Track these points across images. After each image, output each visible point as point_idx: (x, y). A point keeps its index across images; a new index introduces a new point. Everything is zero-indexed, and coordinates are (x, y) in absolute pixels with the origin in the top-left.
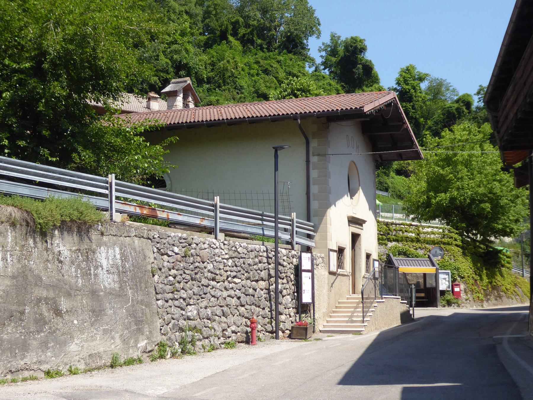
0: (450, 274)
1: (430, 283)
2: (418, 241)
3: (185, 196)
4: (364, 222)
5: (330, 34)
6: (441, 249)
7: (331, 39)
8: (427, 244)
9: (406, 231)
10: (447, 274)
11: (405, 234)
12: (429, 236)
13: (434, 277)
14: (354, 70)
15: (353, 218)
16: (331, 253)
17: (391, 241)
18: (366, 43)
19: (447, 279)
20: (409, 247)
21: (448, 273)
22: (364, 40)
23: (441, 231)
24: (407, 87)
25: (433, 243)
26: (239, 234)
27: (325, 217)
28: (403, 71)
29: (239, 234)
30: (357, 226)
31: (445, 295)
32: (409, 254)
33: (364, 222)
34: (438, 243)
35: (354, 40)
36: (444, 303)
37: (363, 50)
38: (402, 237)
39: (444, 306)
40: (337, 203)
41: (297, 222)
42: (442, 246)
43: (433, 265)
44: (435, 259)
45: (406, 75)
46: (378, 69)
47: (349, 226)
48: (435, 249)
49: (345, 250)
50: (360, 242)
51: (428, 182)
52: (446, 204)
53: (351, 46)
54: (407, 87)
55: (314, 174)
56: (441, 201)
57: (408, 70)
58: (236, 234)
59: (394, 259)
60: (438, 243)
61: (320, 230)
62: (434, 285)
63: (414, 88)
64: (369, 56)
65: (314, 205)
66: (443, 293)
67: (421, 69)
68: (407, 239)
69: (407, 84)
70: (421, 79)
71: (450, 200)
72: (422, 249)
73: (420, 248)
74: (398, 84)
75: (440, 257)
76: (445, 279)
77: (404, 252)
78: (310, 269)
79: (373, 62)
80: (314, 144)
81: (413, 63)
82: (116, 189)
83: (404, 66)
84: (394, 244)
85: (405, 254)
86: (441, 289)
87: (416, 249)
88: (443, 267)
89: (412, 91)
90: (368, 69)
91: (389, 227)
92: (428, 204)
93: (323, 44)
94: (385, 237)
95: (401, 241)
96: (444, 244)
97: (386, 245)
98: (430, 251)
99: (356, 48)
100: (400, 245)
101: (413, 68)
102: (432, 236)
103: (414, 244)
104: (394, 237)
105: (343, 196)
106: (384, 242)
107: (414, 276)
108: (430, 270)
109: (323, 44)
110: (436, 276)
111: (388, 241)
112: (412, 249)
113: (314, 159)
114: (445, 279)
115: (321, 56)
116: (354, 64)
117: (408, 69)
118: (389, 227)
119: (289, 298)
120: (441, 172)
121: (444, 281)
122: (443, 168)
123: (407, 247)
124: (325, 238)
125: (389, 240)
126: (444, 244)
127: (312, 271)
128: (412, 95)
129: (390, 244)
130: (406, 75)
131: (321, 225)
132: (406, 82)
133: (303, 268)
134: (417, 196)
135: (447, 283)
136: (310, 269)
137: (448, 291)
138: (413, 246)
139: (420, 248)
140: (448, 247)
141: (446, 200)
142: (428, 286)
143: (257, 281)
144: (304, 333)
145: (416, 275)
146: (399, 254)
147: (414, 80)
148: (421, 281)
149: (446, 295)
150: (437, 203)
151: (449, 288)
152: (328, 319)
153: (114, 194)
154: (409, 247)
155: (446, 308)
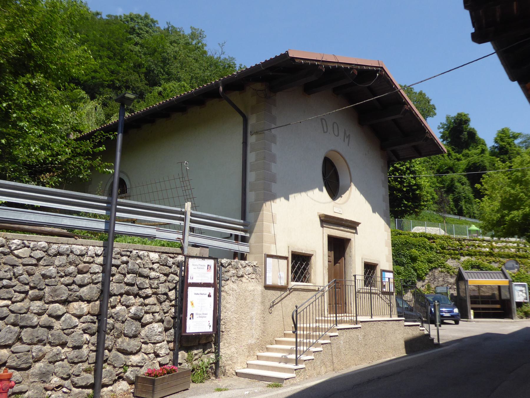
0: (527, 286)
1: (505, 295)
2: (491, 254)
3: (220, 217)
4: (358, 224)
5: (445, 116)
6: (517, 263)
7: (447, 120)
8: (501, 258)
9: (479, 246)
10: (524, 286)
11: (478, 249)
12: (502, 250)
13: (507, 290)
14: (461, 136)
15: (326, 216)
16: (269, 260)
17: (463, 256)
18: (469, 116)
19: (524, 291)
20: (483, 261)
21: (525, 285)
22: (468, 114)
23: (515, 245)
24: (503, 144)
25: (509, 256)
26: (43, 228)
27: (261, 212)
28: (500, 132)
29: (38, 228)
30: (342, 228)
31: (522, 306)
32: (483, 268)
33: (358, 224)
34: (513, 257)
35: (460, 115)
36: (521, 314)
37: (467, 121)
38: (475, 252)
39: (522, 318)
40: (291, 197)
41: (192, 215)
42: (517, 259)
43: (506, 277)
44: (507, 272)
45: (502, 135)
46: (481, 134)
47: (322, 226)
48: (511, 263)
49: (313, 258)
50: (350, 248)
51: (502, 202)
52: (519, 220)
53: (458, 119)
54: (503, 144)
55: (251, 157)
56: (513, 217)
57: (503, 131)
58: (27, 227)
59: (463, 272)
60: (513, 257)
61: (256, 229)
62: (508, 296)
63: (509, 144)
64: (472, 125)
65: (251, 196)
66: (519, 304)
67: (514, 129)
68: (481, 254)
69: (504, 142)
70: (515, 137)
71: (523, 217)
72: (496, 263)
73: (494, 261)
74: (496, 142)
75: (516, 270)
76: (521, 291)
77: (477, 266)
78: (212, 281)
79: (476, 129)
80: (252, 121)
81: (508, 126)
82: (191, 219)
83: (500, 129)
84: (467, 258)
85: (478, 267)
86: (517, 301)
87: (490, 263)
88: (519, 279)
89: (508, 146)
90: (472, 135)
91: (461, 243)
92: (500, 222)
93: (441, 124)
94: (457, 252)
95: (476, 255)
96: (520, 257)
97: (459, 259)
98: (504, 264)
99: (461, 120)
100: (473, 259)
101: (508, 130)
102: (507, 250)
103: (488, 258)
104: (467, 252)
105: (315, 188)
106: (456, 256)
107: (489, 288)
108: (503, 282)
109: (441, 124)
110: (510, 289)
111: (461, 256)
112: (486, 263)
113: (252, 139)
114: (521, 291)
115: (440, 132)
116: (461, 132)
117: (503, 131)
118: (461, 243)
119: (158, 327)
120: (512, 191)
121: (521, 293)
122: (513, 188)
123: (480, 261)
124: (261, 240)
125: (462, 254)
126: (520, 257)
127: (217, 286)
128: (507, 149)
129: (463, 259)
130: (502, 135)
131: (257, 223)
132: (502, 140)
133: (190, 281)
134: (491, 215)
135: (524, 295)
136: (212, 281)
137: (526, 303)
138: (487, 260)
139: (494, 261)
140: (524, 260)
141: (518, 216)
142: (503, 297)
143: (65, 302)
144: (151, 389)
145: (491, 288)
146: (472, 268)
147: (509, 138)
148: (496, 292)
149: (524, 306)
150: (511, 220)
151: (527, 300)
152: (259, 354)
153: (189, 224)
154: (483, 261)
155: (524, 320)
